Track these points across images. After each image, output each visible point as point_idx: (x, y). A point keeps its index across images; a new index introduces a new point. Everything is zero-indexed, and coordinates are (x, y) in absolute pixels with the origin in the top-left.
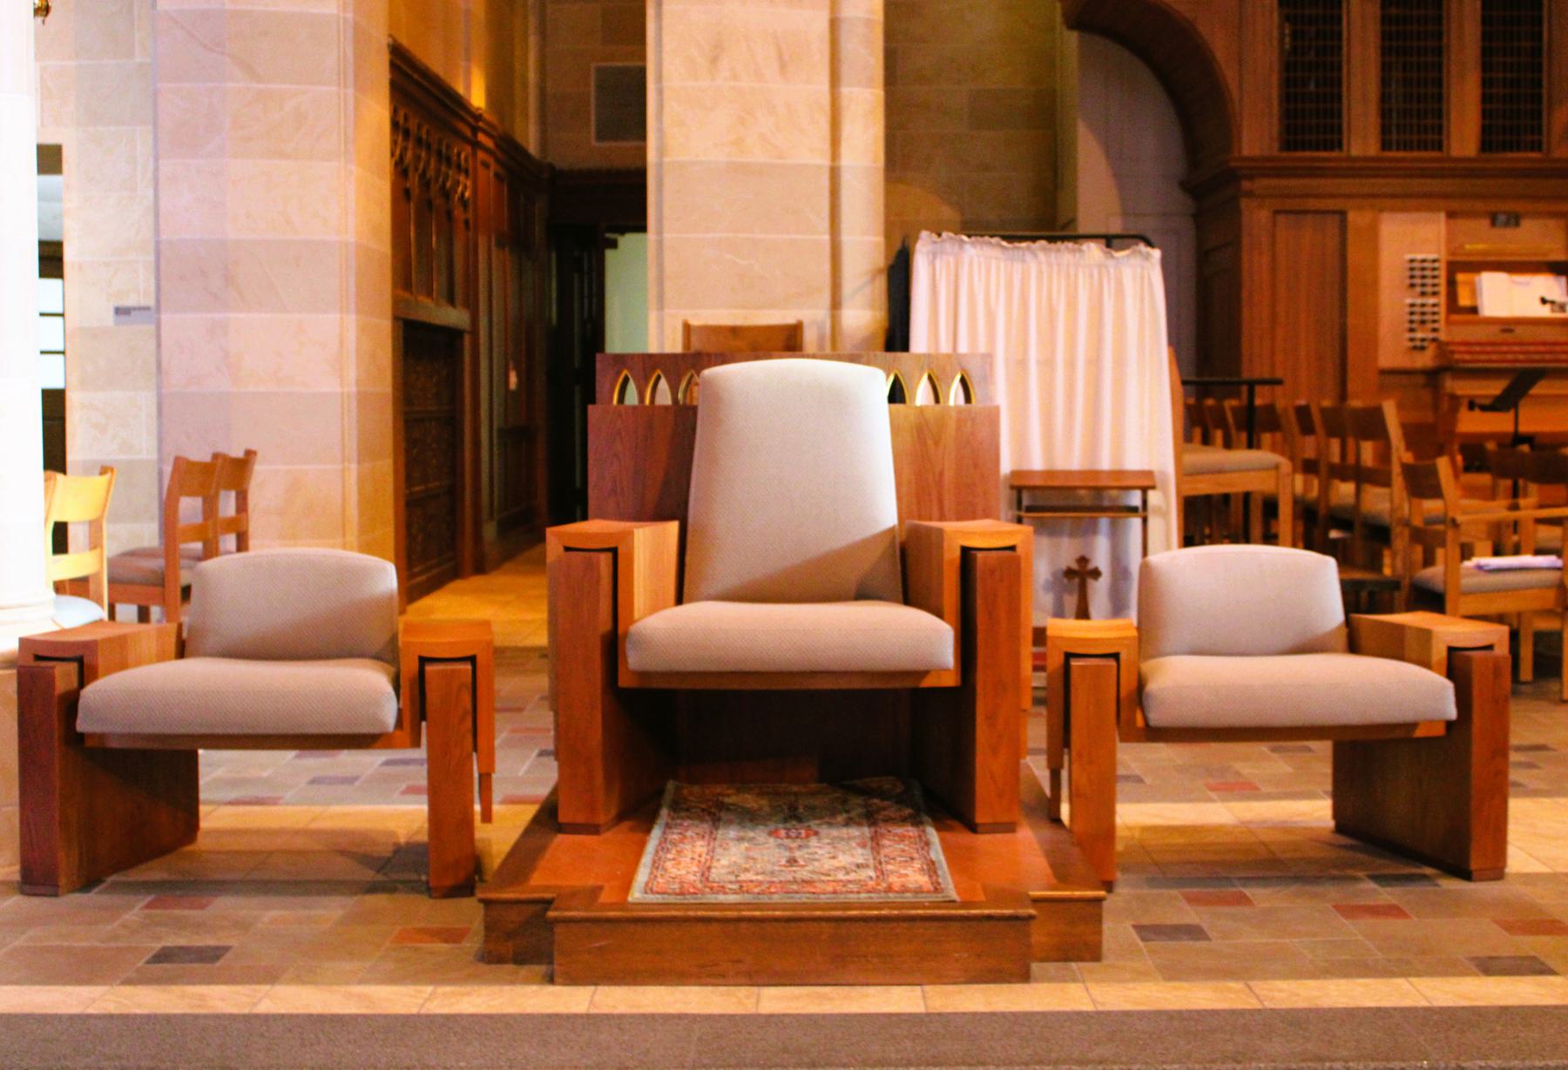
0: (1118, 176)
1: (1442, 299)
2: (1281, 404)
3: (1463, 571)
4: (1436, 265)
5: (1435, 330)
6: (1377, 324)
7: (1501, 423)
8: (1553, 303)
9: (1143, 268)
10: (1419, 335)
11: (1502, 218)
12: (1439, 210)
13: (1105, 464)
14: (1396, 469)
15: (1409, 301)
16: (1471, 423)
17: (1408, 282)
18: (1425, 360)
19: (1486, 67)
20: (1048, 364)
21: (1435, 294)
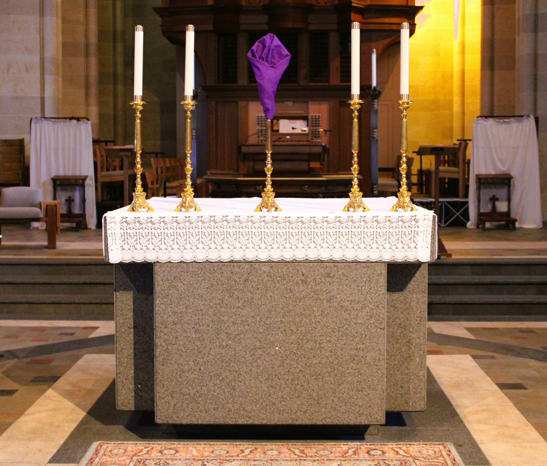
10: (261, 138)
15: (258, 128)
17: (257, 122)
20: (63, 149)
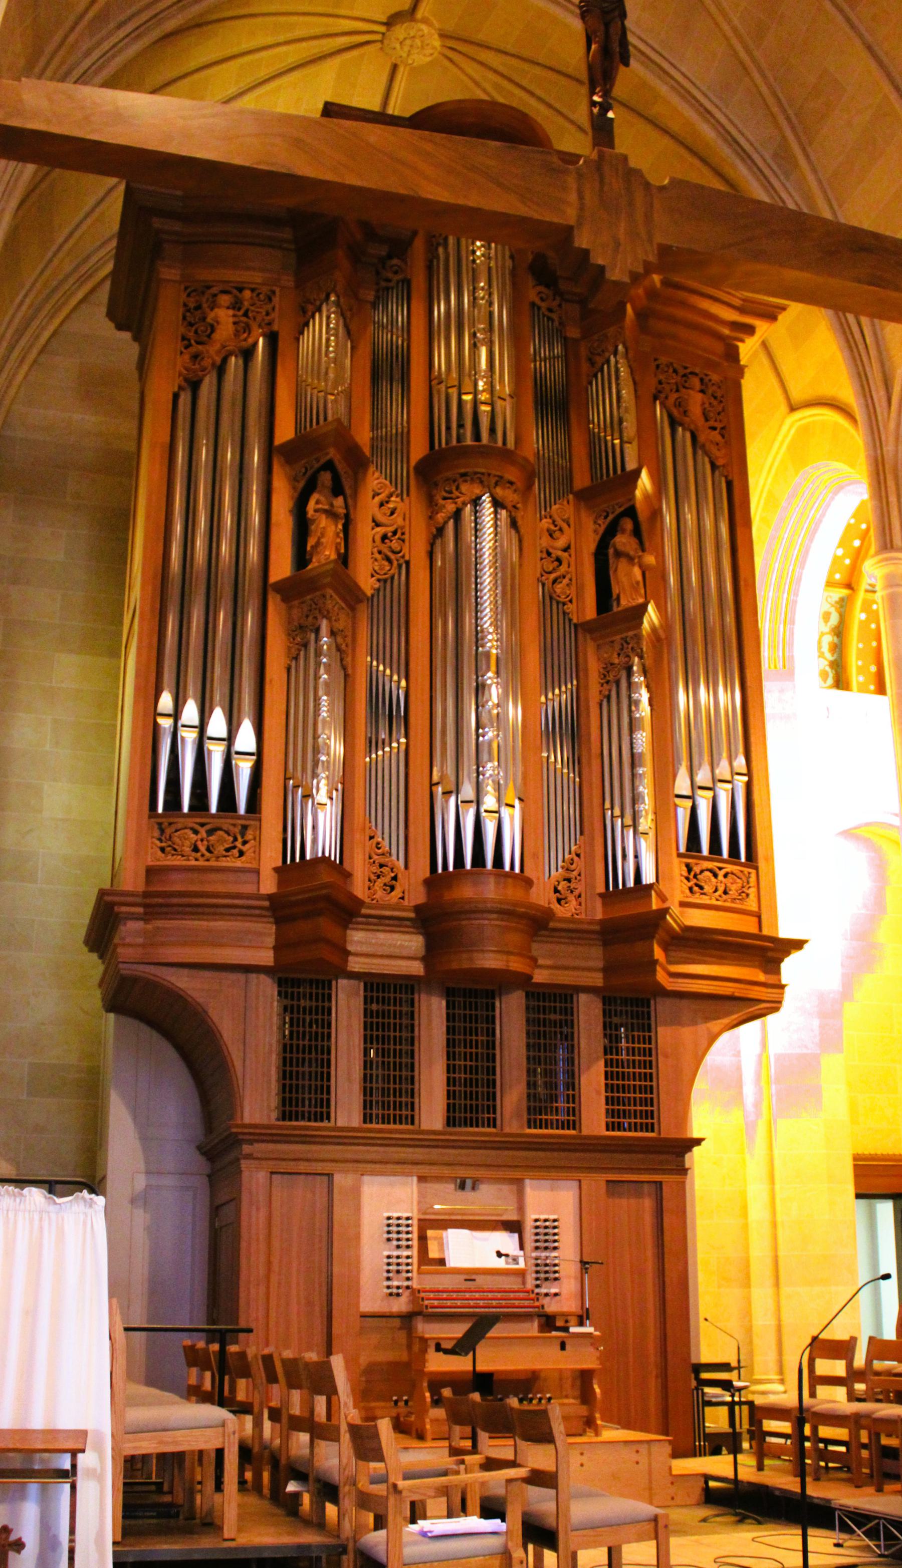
0: (144, 1139)
1: (414, 1252)
2: (251, 1352)
3: (405, 1539)
4: (410, 1222)
5: (408, 1279)
6: (358, 1272)
7: (461, 1364)
8: (507, 1255)
9: (85, 1214)
10: (396, 1283)
11: (469, 1183)
12: (410, 1174)
13: (37, 1423)
14: (344, 1428)
15: (386, 1253)
16: (437, 1363)
18: (401, 1305)
19: (450, 1056)
21: (408, 1247)
